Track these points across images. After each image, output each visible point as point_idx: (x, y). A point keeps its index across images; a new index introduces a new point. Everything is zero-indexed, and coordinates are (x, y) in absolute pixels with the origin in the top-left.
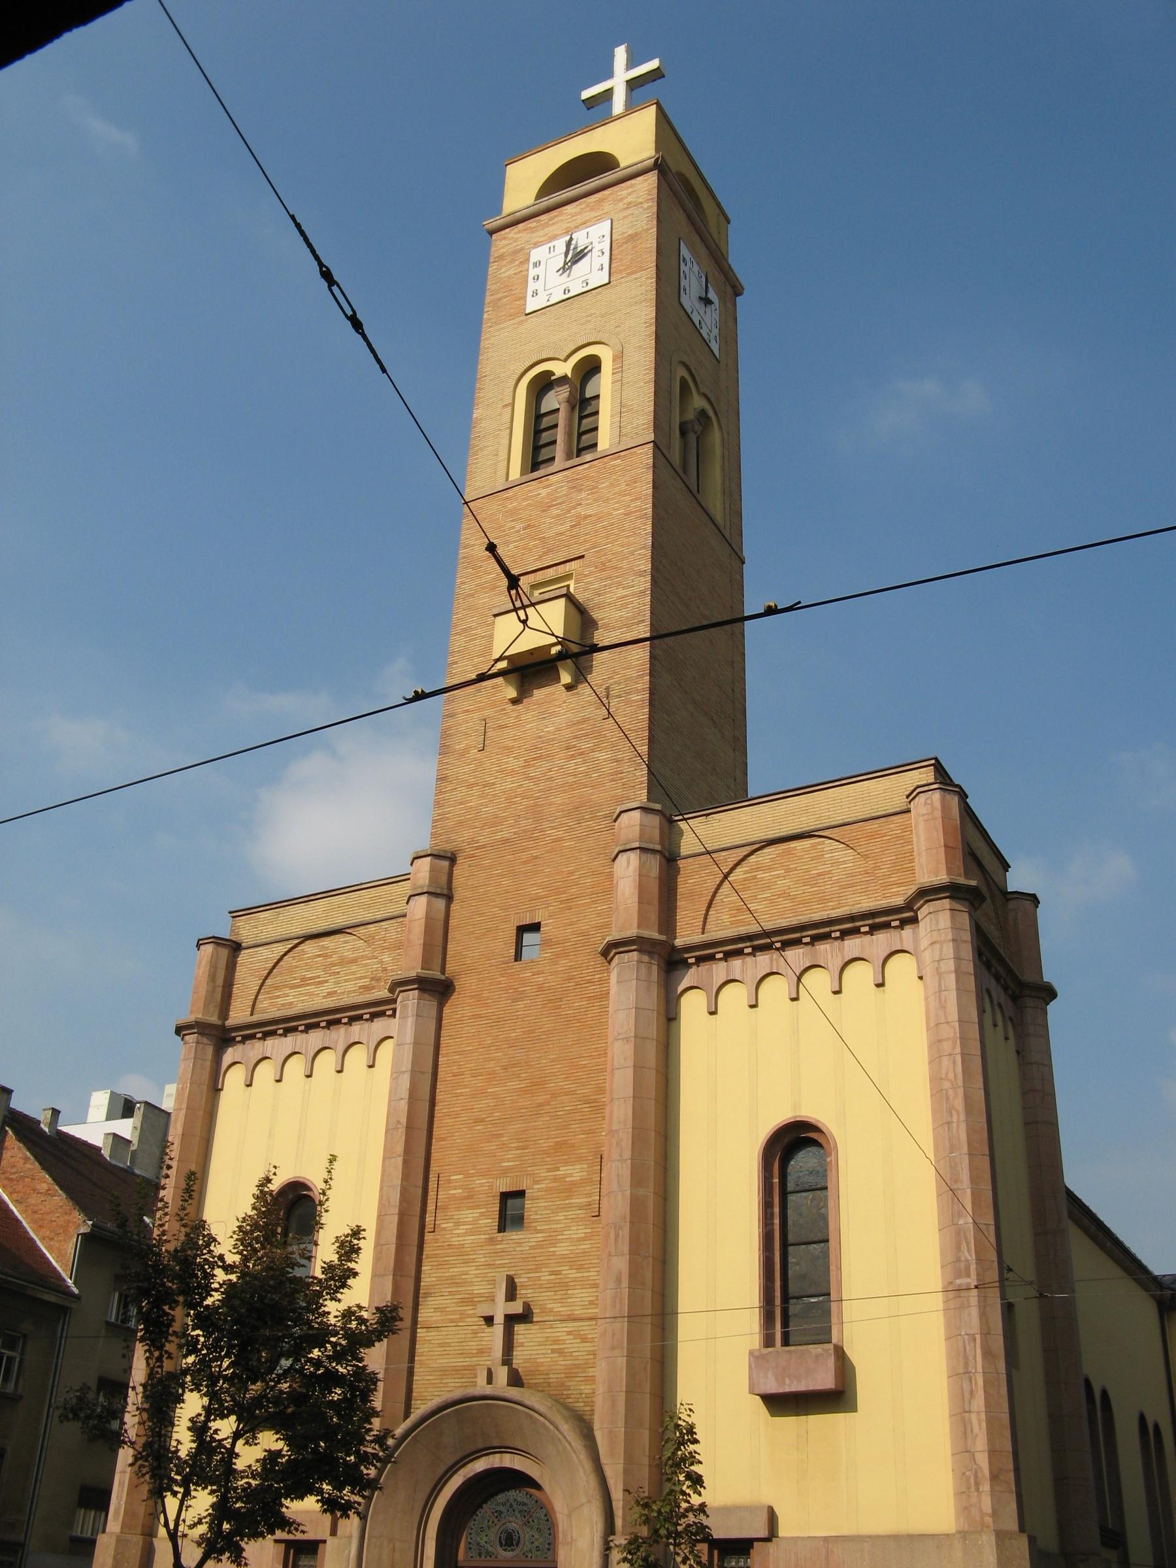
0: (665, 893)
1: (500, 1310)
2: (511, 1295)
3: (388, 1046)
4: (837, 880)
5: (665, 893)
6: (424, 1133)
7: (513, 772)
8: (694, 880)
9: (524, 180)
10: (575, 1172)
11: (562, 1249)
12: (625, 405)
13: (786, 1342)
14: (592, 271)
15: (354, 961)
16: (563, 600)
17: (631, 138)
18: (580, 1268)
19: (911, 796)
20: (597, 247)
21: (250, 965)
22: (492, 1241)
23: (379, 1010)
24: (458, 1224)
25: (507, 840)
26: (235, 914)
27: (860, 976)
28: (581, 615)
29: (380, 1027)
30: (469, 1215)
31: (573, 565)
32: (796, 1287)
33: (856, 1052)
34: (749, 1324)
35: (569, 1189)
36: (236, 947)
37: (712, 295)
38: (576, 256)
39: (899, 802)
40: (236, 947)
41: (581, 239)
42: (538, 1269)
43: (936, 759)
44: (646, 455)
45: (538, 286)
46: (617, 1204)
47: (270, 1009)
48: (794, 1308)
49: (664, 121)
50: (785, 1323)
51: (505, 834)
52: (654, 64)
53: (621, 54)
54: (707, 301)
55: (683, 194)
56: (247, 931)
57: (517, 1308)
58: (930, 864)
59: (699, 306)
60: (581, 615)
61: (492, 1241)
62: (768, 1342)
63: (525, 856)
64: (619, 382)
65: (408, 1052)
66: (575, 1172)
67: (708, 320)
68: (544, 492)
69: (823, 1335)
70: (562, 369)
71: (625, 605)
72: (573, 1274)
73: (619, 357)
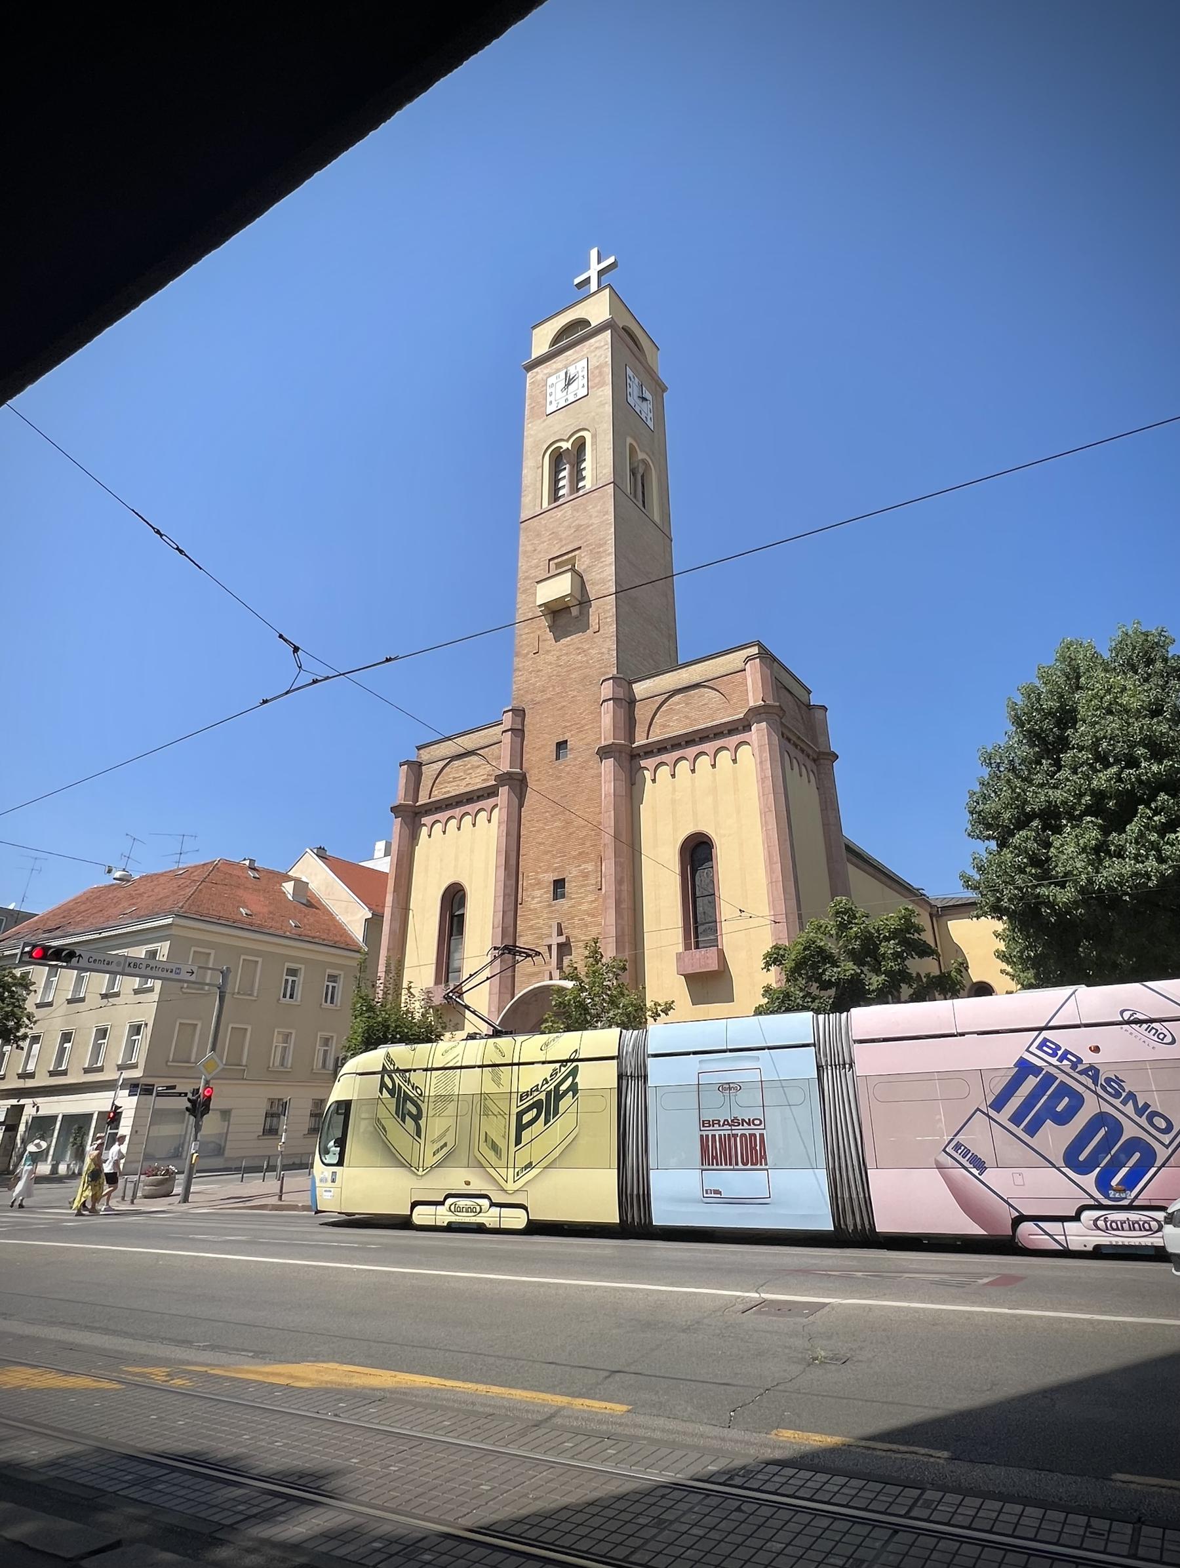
0: (629, 724)
1: (555, 940)
2: (560, 933)
3: (497, 810)
4: (711, 710)
5: (629, 724)
6: (515, 853)
7: (550, 664)
8: (642, 713)
9: (541, 340)
10: (590, 867)
11: (585, 907)
12: (598, 465)
13: (697, 947)
14: (578, 388)
15: (479, 766)
16: (569, 574)
17: (597, 310)
18: (593, 916)
19: (746, 661)
20: (581, 374)
21: (429, 772)
22: (550, 906)
23: (491, 792)
24: (533, 898)
25: (549, 699)
26: (419, 748)
27: (724, 757)
28: (580, 581)
29: (491, 802)
30: (538, 893)
31: (577, 552)
32: (700, 920)
33: (727, 797)
34: (678, 935)
35: (586, 876)
36: (420, 764)
37: (647, 395)
38: (569, 381)
39: (741, 665)
40: (420, 764)
41: (572, 371)
42: (573, 918)
43: (760, 645)
44: (610, 489)
45: (552, 390)
46: (609, 886)
47: (438, 795)
48: (700, 929)
49: (614, 293)
50: (696, 936)
51: (549, 696)
52: (611, 260)
53: (594, 253)
54: (644, 399)
55: (628, 341)
56: (425, 755)
57: (562, 939)
58: (753, 690)
59: (639, 401)
60: (580, 581)
61: (550, 906)
62: (687, 947)
63: (559, 706)
64: (596, 461)
65: (505, 811)
66: (590, 867)
67: (645, 409)
68: (559, 514)
69: (714, 943)
70: (566, 445)
71: (603, 575)
72: (589, 919)
73: (594, 436)
